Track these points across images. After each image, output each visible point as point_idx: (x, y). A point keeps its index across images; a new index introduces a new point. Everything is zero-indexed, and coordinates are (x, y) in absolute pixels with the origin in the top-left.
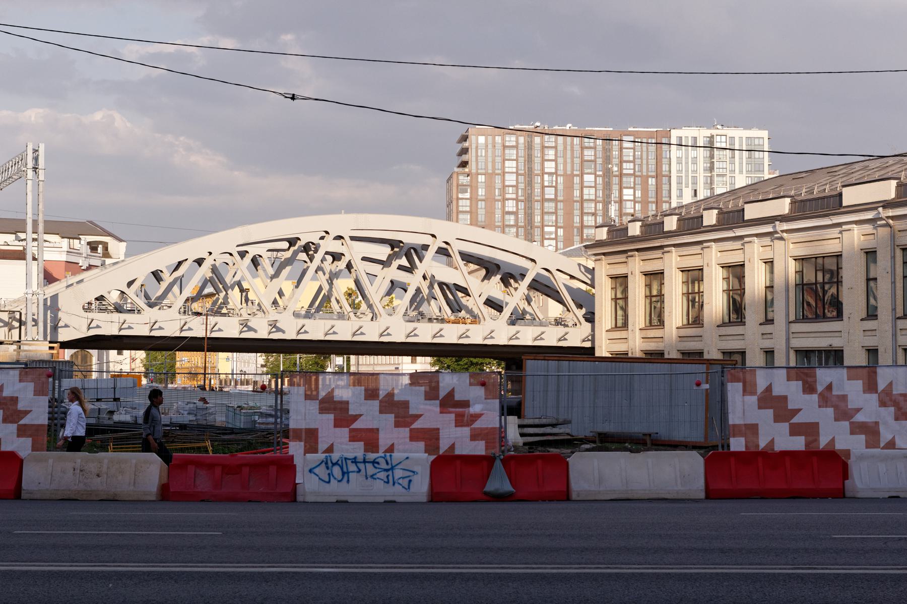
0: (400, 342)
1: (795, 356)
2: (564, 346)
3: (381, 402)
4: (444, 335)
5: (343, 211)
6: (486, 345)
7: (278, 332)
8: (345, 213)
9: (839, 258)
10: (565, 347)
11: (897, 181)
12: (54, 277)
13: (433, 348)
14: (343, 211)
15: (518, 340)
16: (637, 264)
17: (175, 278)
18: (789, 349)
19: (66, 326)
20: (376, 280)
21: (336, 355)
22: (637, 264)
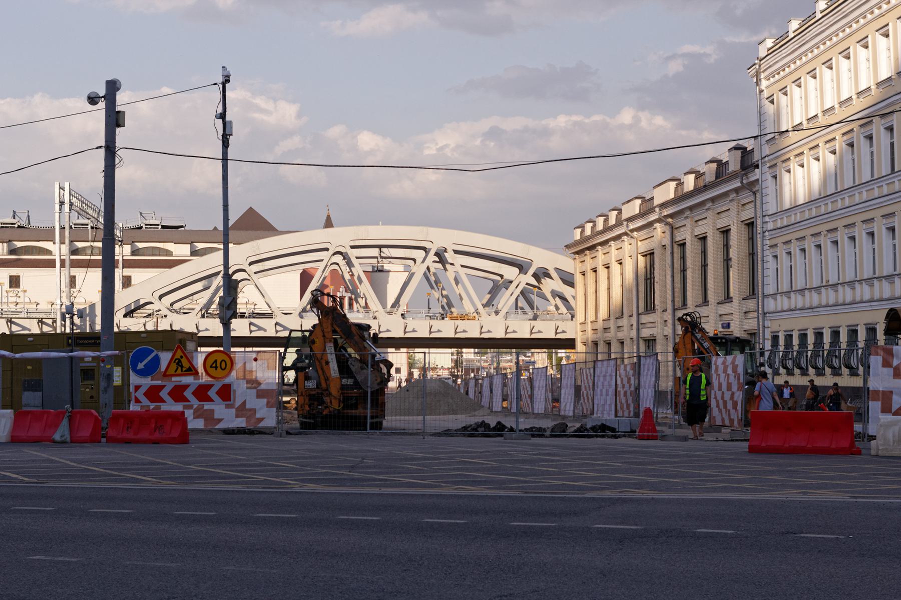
0: (398, 337)
1: (621, 346)
2: (562, 338)
3: (894, 369)
4: (491, 331)
5: (380, 223)
6: (483, 339)
7: (260, 330)
8: (383, 224)
9: (93, 240)
10: (563, 339)
11: (676, 182)
12: (386, 286)
13: (509, 342)
14: (380, 223)
15: (490, 333)
16: (578, 265)
17: (564, 284)
18: (675, 336)
19: (171, 325)
20: (896, 285)
21: (119, 355)
22: (578, 265)
